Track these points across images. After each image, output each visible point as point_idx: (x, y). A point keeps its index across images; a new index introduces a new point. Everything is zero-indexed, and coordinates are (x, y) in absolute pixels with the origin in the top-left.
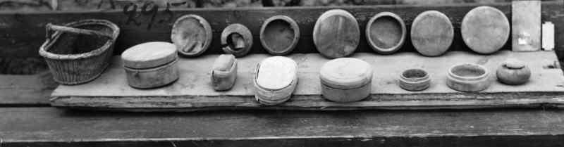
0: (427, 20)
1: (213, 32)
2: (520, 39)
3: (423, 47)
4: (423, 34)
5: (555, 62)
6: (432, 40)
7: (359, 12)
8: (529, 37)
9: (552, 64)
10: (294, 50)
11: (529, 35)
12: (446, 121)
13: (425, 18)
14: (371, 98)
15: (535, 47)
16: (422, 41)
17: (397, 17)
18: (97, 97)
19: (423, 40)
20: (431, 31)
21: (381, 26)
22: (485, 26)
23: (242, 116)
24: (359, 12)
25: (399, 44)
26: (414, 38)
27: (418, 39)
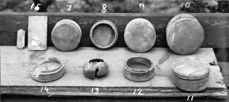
0: (65, 27)
1: (118, 34)
2: (33, 41)
3: (58, 44)
4: (60, 36)
5: (214, 61)
6: (64, 40)
7: (82, 18)
8: (39, 41)
9: (212, 62)
10: (114, 45)
11: (39, 39)
12: (198, 94)
13: (63, 25)
14: (85, 90)
15: (42, 47)
16: (58, 40)
17: (114, 28)
18: (20, 87)
19: (59, 39)
20: (66, 35)
21: (98, 33)
22: (142, 36)
23: (134, 96)
24: (82, 18)
25: (111, 44)
26: (53, 37)
27: (56, 38)
